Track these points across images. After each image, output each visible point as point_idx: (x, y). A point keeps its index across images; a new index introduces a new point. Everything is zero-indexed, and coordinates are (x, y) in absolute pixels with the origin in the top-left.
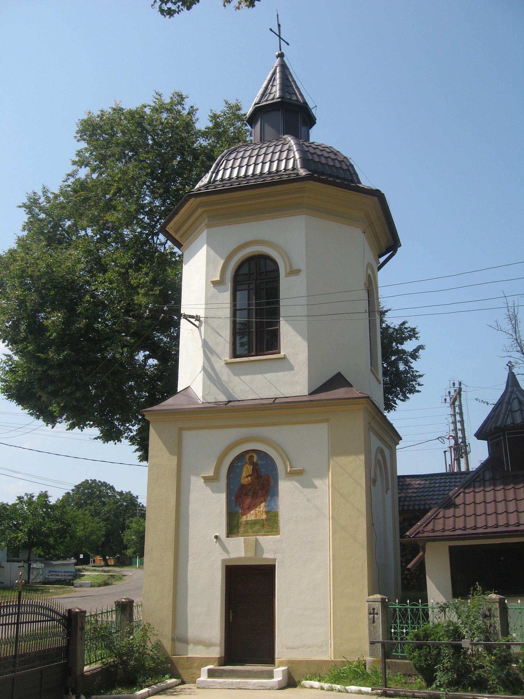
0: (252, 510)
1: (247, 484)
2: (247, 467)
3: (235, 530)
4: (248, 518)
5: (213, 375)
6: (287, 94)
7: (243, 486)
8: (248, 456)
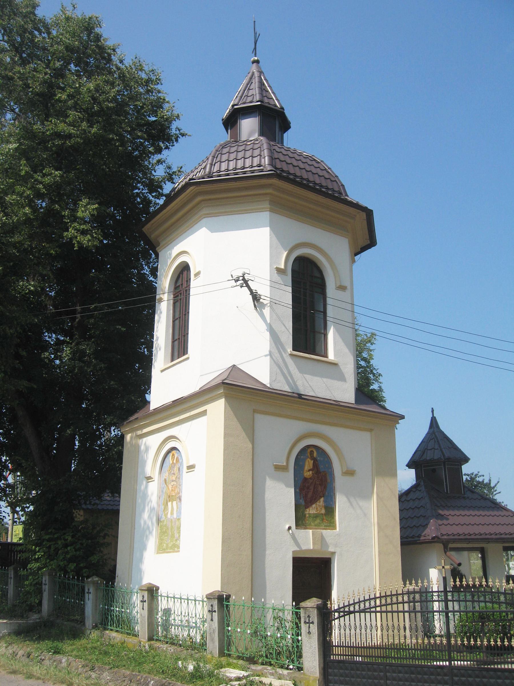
0: (313, 504)
1: (309, 477)
2: (309, 461)
3: (148, 532)
4: (311, 511)
5: (291, 381)
6: (265, 98)
7: (305, 479)
8: (309, 450)
